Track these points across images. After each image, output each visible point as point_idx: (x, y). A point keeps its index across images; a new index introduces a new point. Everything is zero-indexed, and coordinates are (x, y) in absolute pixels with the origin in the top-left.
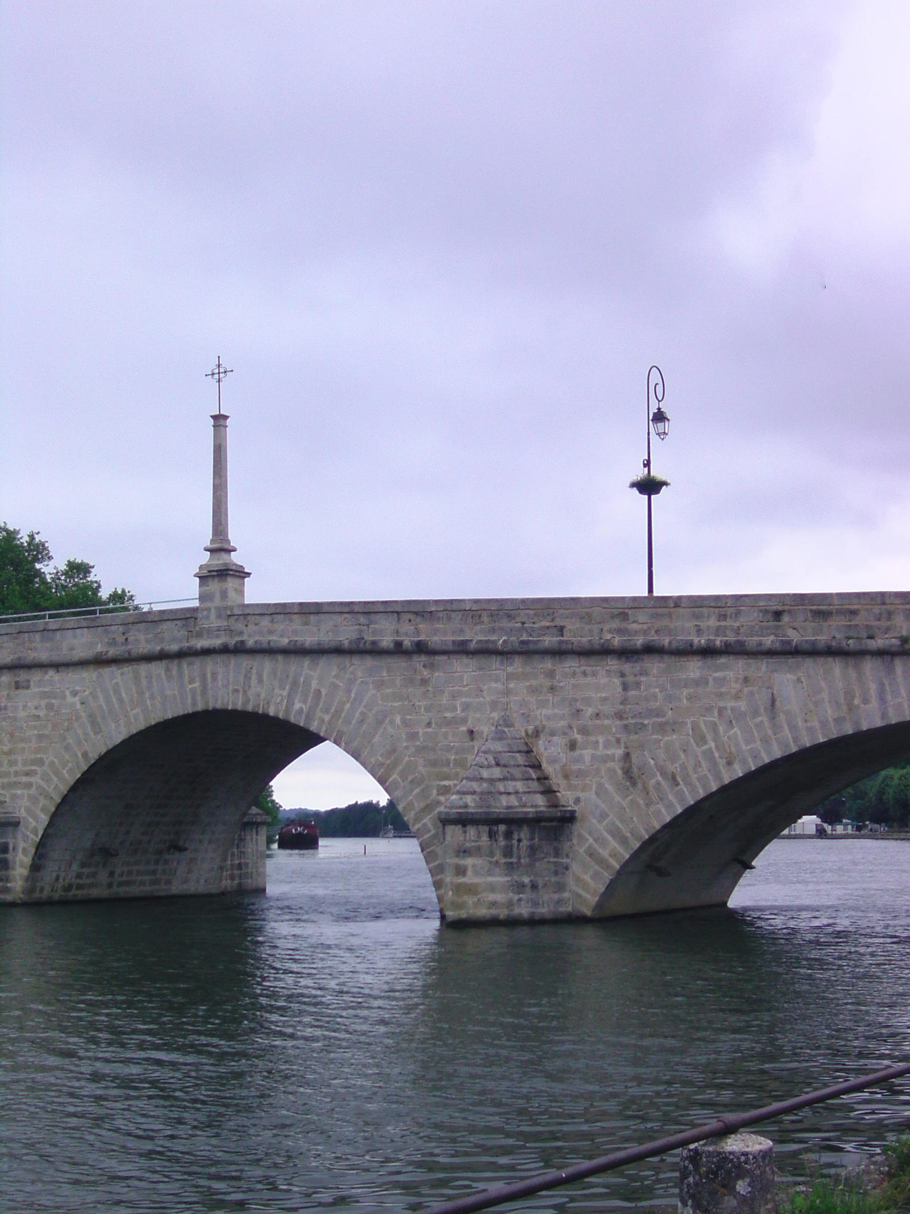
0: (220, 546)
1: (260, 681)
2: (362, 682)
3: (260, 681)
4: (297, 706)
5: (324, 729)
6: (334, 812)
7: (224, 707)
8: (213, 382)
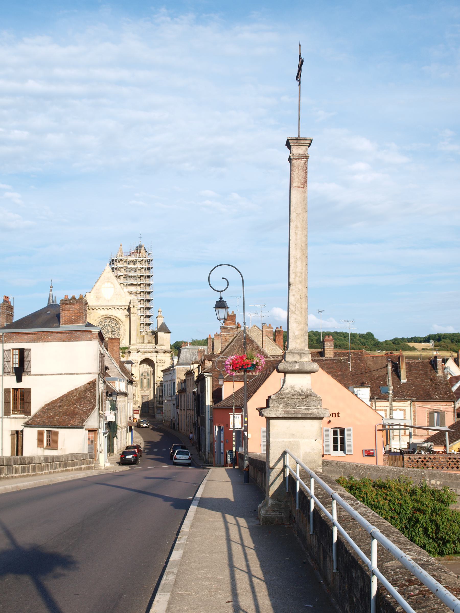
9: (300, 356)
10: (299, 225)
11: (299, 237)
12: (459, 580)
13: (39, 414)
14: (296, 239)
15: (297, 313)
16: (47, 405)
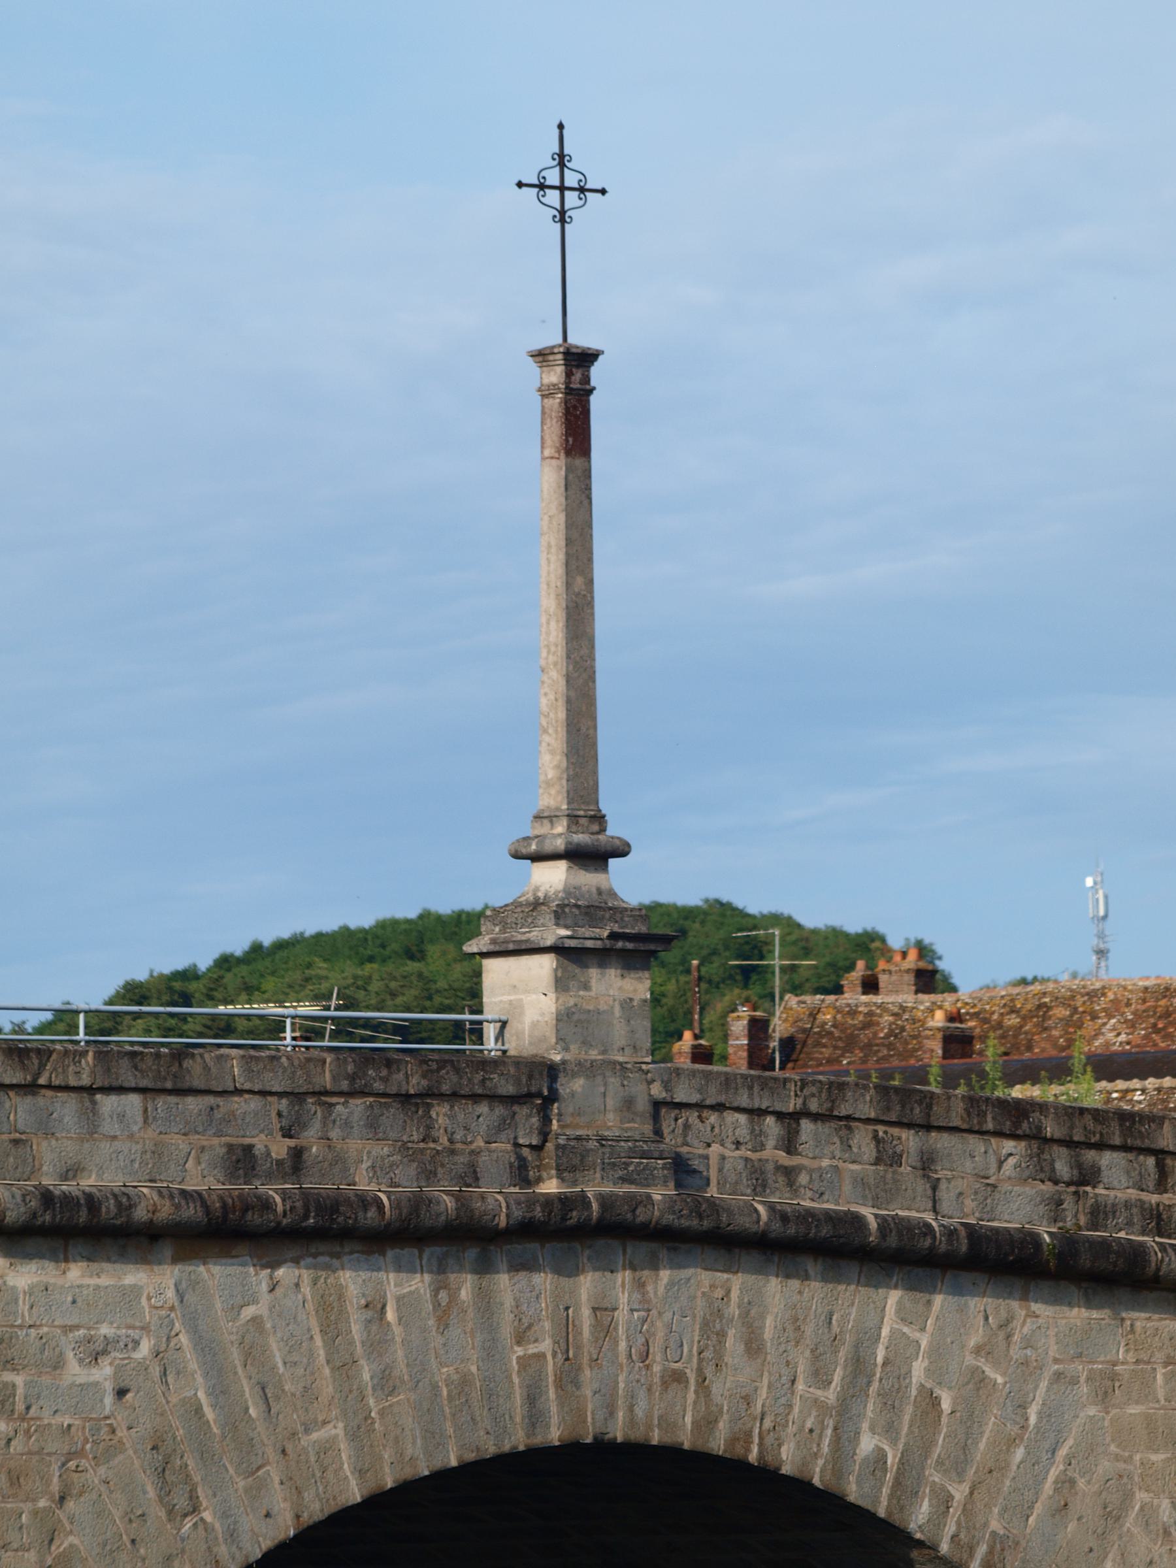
0: (584, 807)
1: (753, 1347)
2: (1058, 1376)
3: (753, 1347)
4: (867, 1444)
5: (950, 1528)
6: (319, 936)
7: (637, 1435)
8: (537, 214)
9: (551, 822)
10: (553, 543)
11: (552, 566)
12: (5, 1137)
13: (826, 938)
14: (549, 573)
15: (550, 731)
16: (790, 918)
